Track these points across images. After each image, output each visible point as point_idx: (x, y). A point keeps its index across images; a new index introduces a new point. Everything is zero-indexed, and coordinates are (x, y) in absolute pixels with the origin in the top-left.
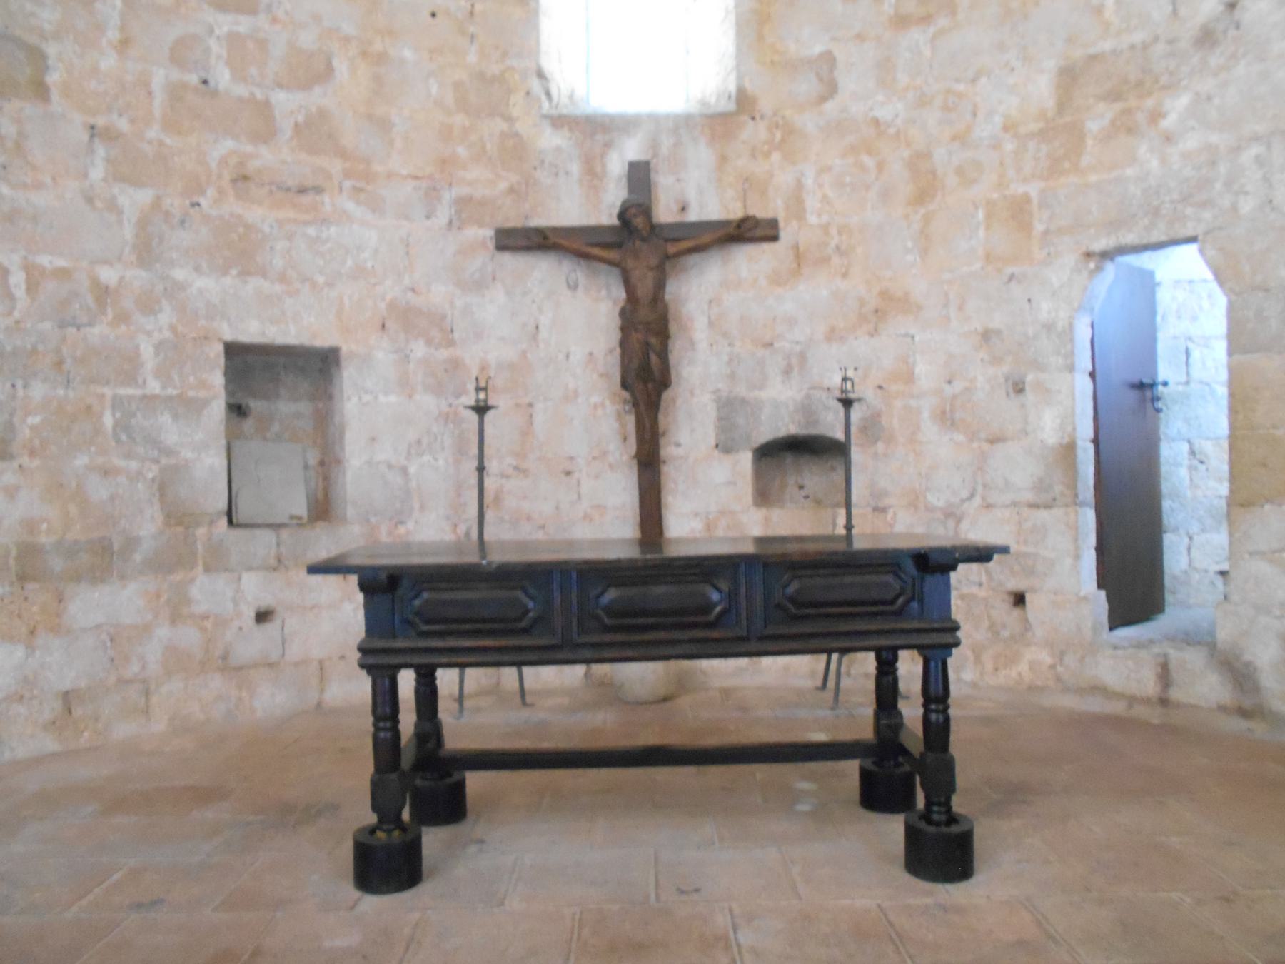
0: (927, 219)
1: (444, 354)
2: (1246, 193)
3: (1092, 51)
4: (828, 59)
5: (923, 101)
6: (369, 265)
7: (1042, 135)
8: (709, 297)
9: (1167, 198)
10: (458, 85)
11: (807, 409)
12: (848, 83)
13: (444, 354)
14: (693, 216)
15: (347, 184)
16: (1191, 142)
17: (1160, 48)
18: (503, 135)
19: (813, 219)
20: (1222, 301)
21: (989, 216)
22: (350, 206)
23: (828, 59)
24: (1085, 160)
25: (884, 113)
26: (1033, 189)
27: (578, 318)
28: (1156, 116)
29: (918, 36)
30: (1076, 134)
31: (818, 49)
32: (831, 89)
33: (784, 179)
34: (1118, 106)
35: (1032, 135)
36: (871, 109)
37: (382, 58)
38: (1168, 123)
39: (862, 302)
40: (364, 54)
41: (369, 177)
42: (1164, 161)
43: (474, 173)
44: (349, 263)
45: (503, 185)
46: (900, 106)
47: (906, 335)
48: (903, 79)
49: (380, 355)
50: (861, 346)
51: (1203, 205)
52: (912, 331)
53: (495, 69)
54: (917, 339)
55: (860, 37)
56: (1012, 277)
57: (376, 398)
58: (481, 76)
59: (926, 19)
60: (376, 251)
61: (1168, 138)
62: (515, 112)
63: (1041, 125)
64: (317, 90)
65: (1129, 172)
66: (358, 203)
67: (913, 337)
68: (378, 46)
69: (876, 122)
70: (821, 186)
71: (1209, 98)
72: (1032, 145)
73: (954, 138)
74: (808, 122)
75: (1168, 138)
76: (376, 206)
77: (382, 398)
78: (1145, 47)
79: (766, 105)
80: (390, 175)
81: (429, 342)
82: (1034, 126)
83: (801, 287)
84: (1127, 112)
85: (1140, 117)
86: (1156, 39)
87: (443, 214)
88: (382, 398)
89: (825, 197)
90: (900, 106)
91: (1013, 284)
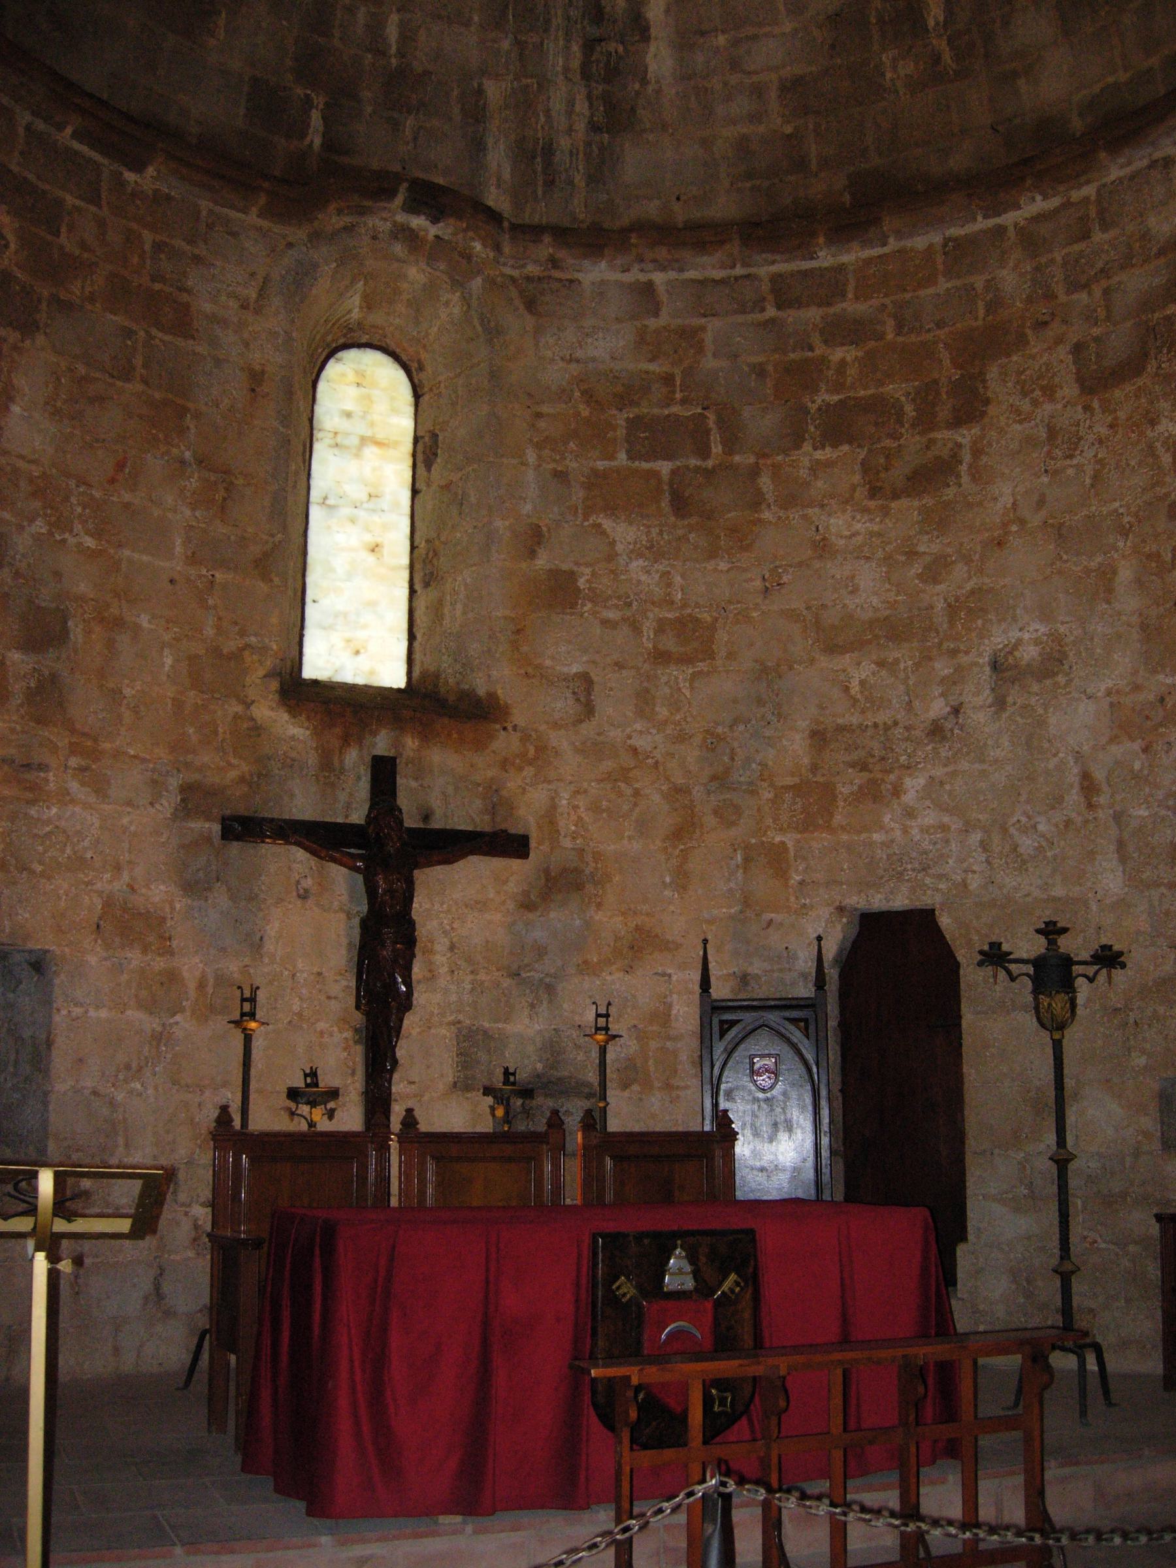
0: (685, 855)
1: (160, 964)
2: (974, 872)
3: (840, 721)
4: (586, 679)
5: (681, 738)
6: (88, 856)
7: (796, 789)
8: (456, 906)
9: (909, 866)
10: (192, 659)
11: (552, 1049)
12: (606, 709)
13: (160, 964)
14: (437, 824)
15: (74, 762)
16: (930, 818)
17: (898, 732)
18: (236, 717)
19: (567, 843)
20: (398, 802)
21: (747, 860)
22: (74, 786)
23: (586, 679)
24: (838, 819)
25: (640, 742)
26: (789, 839)
27: (309, 922)
28: (897, 791)
29: (679, 674)
30: (828, 792)
31: (575, 669)
32: (589, 710)
33: (538, 796)
34: (865, 775)
35: (787, 788)
36: (630, 737)
37: (118, 623)
38: (909, 798)
39: (617, 939)
40: (102, 620)
41: (95, 754)
42: (905, 831)
43: (205, 757)
44: (68, 851)
45: (233, 774)
46: (659, 738)
47: (664, 975)
48: (663, 712)
49: (93, 960)
50: (615, 981)
51: (940, 877)
52: (669, 971)
53: (230, 646)
54: (674, 978)
55: (619, 666)
56: (770, 923)
57: (86, 1012)
58: (216, 652)
59: (686, 660)
60: (98, 841)
61: (910, 813)
62: (252, 694)
63: (797, 780)
64: (52, 653)
65: (876, 837)
66: (83, 784)
67: (670, 976)
68: (114, 611)
69: (635, 751)
70: (576, 807)
71: (942, 783)
72: (788, 796)
73: (714, 778)
74: (560, 740)
75: (910, 813)
76: (100, 787)
77: (92, 1013)
78: (887, 728)
79: (519, 717)
80: (117, 754)
81: (145, 950)
82: (789, 781)
83: (552, 915)
84: (873, 782)
85: (886, 787)
86: (896, 723)
87: (168, 804)
88: (92, 1013)
89: (580, 818)
90: (659, 738)
91: (771, 930)
